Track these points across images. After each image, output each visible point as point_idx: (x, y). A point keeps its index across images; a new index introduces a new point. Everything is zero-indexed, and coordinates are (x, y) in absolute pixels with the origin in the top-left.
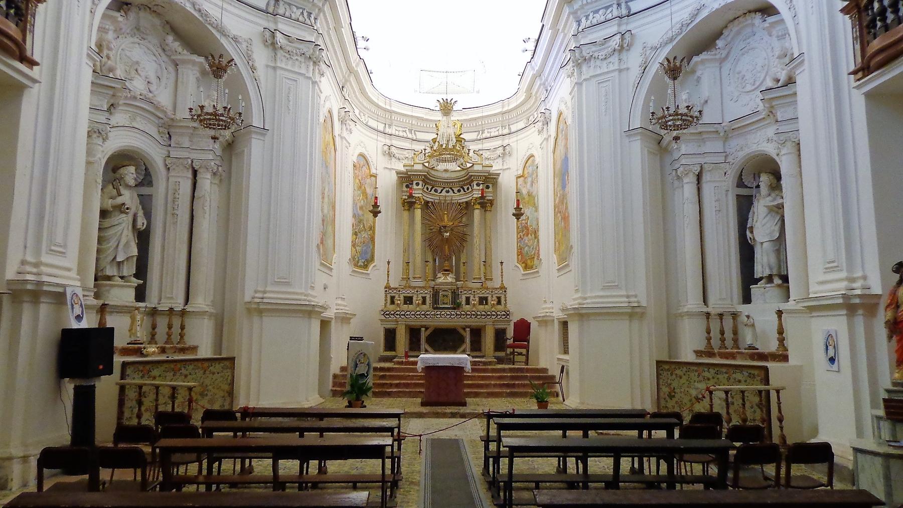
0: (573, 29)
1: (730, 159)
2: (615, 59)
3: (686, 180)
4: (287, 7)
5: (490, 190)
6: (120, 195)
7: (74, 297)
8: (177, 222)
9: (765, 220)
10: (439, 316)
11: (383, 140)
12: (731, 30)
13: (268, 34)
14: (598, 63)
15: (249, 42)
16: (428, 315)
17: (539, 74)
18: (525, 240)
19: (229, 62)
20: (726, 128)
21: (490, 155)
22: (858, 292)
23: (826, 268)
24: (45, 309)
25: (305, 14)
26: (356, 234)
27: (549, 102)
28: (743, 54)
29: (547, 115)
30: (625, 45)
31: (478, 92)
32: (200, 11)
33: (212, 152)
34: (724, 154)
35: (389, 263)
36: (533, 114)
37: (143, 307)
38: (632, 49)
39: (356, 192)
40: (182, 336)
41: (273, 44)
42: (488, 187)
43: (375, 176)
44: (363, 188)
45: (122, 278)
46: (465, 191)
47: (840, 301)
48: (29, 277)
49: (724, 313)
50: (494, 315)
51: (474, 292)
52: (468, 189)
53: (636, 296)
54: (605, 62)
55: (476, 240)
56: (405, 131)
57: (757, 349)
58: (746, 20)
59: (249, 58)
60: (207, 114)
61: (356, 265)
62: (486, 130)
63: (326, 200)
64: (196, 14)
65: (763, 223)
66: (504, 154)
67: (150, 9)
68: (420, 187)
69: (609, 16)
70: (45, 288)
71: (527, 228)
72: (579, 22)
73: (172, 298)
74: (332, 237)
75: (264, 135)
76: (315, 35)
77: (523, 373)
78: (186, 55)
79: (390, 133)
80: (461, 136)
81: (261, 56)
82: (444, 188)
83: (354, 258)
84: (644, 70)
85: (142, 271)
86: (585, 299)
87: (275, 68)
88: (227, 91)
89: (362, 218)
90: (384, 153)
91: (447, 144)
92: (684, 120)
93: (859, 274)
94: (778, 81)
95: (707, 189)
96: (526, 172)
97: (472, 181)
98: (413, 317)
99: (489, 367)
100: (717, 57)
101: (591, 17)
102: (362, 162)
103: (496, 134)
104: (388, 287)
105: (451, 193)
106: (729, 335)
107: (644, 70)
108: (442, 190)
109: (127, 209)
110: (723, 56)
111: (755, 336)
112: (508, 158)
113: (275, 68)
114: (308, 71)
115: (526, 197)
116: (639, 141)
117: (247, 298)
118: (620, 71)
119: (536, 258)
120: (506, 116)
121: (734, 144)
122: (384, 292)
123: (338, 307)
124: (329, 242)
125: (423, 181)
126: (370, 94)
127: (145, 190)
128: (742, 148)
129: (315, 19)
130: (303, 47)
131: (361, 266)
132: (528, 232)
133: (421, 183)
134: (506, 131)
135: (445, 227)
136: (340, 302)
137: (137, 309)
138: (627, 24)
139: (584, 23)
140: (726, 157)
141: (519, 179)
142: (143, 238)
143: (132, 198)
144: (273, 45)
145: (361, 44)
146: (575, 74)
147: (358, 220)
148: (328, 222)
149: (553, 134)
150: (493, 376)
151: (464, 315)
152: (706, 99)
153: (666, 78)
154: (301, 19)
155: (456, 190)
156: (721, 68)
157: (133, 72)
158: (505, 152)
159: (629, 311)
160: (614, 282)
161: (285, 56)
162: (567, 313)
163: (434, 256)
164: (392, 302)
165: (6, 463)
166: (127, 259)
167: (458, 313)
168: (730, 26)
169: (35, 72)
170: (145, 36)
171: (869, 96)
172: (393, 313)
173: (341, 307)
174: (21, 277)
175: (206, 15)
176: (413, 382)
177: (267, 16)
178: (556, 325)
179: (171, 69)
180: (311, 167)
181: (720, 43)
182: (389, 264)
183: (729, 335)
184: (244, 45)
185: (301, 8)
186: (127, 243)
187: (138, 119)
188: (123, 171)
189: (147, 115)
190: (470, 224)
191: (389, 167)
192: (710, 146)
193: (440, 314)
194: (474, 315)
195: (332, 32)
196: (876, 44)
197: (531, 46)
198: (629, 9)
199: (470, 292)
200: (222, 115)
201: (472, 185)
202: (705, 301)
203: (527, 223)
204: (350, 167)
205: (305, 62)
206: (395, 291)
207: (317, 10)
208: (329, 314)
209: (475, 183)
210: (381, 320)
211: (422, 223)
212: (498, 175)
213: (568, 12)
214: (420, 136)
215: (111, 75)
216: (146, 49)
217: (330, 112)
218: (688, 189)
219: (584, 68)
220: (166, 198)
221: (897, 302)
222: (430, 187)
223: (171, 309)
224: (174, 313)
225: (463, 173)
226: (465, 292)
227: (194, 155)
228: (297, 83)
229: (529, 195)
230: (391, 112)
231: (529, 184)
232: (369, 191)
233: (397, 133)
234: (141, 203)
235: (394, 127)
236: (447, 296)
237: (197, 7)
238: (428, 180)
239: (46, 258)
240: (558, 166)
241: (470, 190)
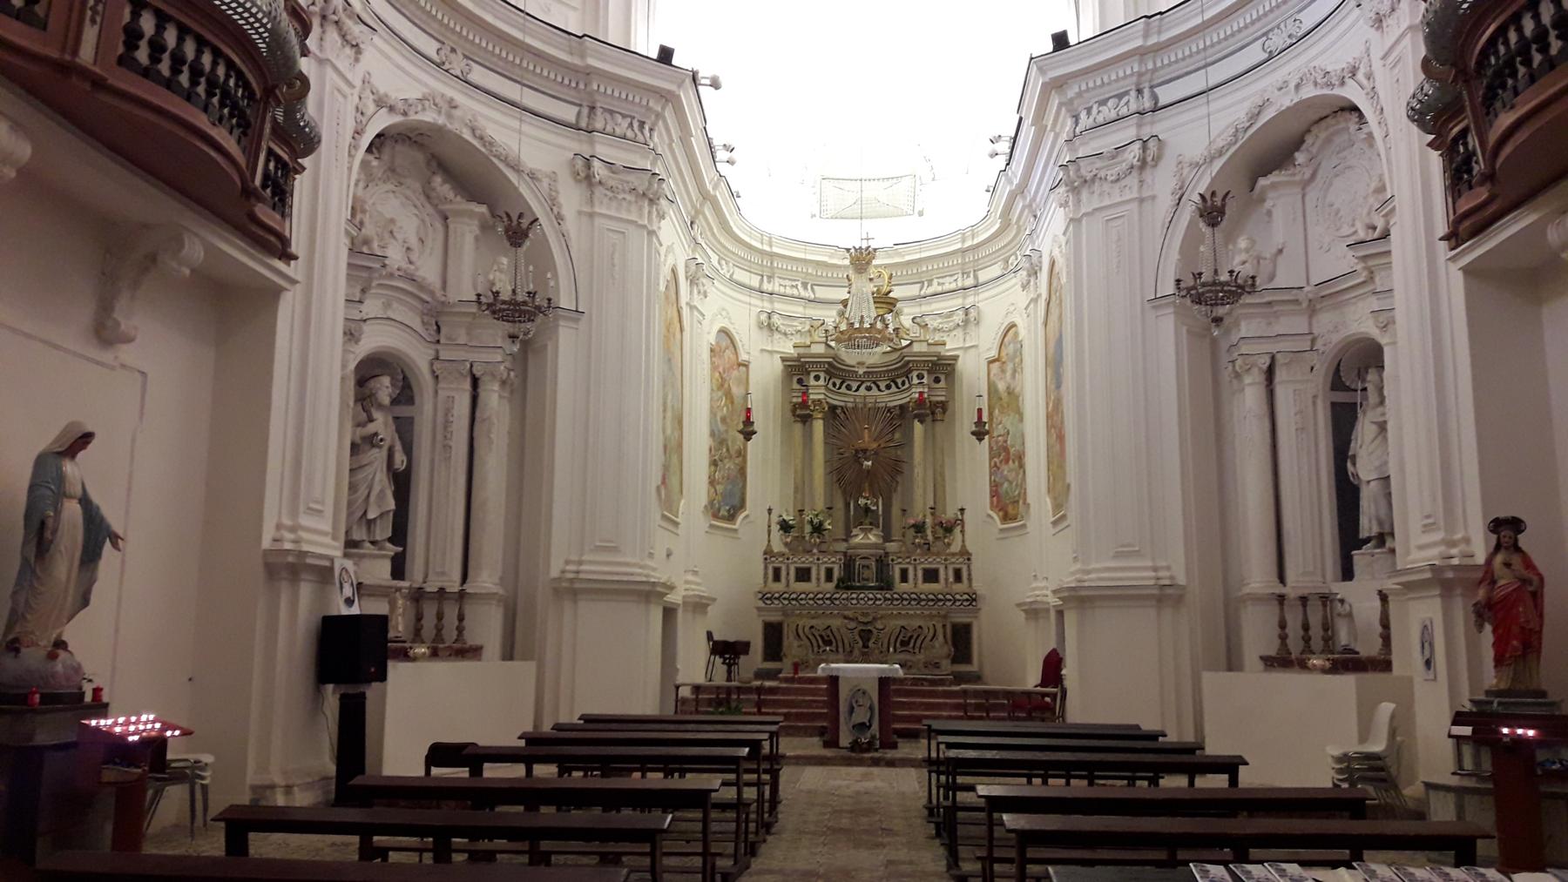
0: (1067, 129)
1: (1318, 345)
2: (1133, 180)
3: (1248, 380)
4: (608, 116)
5: (942, 384)
6: (371, 420)
7: (344, 573)
8: (450, 457)
9: (1373, 446)
10: (854, 602)
11: (758, 303)
12: (1317, 136)
13: (580, 163)
14: (1106, 187)
15: (553, 177)
16: (836, 599)
17: (1021, 190)
18: (1003, 471)
19: (532, 223)
20: (1310, 296)
21: (941, 323)
22: (1455, 561)
23: (1425, 526)
24: (306, 590)
25: (636, 125)
26: (714, 463)
27: (1038, 237)
28: (1337, 175)
29: (1035, 259)
30: (1149, 159)
31: (921, 214)
32: (481, 138)
33: (499, 350)
34: (1310, 337)
35: (770, 511)
36: (1015, 254)
37: (406, 588)
38: (1162, 164)
39: (714, 395)
40: (460, 630)
41: (589, 178)
42: (937, 380)
43: (746, 365)
44: (726, 386)
45: (373, 543)
46: (898, 388)
47: (1428, 575)
48: (288, 546)
49: (1310, 597)
50: (950, 600)
51: (915, 560)
52: (903, 383)
53: (1168, 568)
54: (1118, 184)
55: (918, 471)
56: (796, 287)
57: (1357, 653)
58: (1338, 123)
59: (552, 202)
60: (504, 302)
61: (716, 516)
62: (935, 280)
63: (669, 414)
64: (475, 142)
65: (1370, 450)
66: (966, 322)
67: (410, 138)
68: (821, 382)
69: (1124, 111)
70: (309, 561)
71: (1006, 450)
72: (1076, 118)
73: (443, 573)
74: (678, 473)
75: (577, 320)
76: (651, 157)
77: (998, 699)
78: (461, 204)
79: (770, 289)
80: (891, 295)
81: (571, 199)
82: (863, 382)
83: (711, 503)
84: (1180, 199)
85: (400, 534)
86: (1088, 572)
87: (591, 215)
88: (531, 268)
89: (724, 436)
90: (760, 325)
91: (862, 322)
92: (1226, 292)
93: (1459, 536)
94: (1374, 228)
95: (1281, 393)
96: (1003, 354)
97: (910, 371)
98: (811, 602)
99: (940, 688)
100: (1297, 178)
101: (1094, 111)
102: (725, 342)
103: (953, 286)
104: (768, 553)
105: (875, 391)
106: (1316, 632)
107: (1180, 199)
108: (859, 387)
109: (381, 440)
110: (1307, 176)
111: (1353, 633)
112: (973, 328)
113: (591, 215)
114: (641, 216)
115: (1005, 396)
116: (1172, 316)
117: (554, 573)
118: (1141, 200)
119: (1021, 502)
120: (969, 257)
121: (1325, 322)
122: (762, 560)
123: (688, 586)
124: (674, 481)
125: (827, 372)
126: (735, 229)
127: (403, 411)
128: (1336, 327)
129: (651, 130)
130: (632, 178)
131: (723, 518)
132: (1007, 456)
133: (822, 375)
134: (970, 282)
135: (865, 451)
136: (690, 577)
137: (399, 589)
138: (1152, 123)
139: (1085, 120)
140: (1313, 341)
141: (991, 365)
142: (402, 483)
143: (386, 424)
144: (586, 177)
145: (722, 155)
146: (1070, 203)
147: (719, 440)
148: (673, 448)
149: (1044, 295)
150: (946, 704)
151: (897, 599)
152: (1280, 247)
153: (1202, 225)
154: (630, 134)
155: (882, 385)
156: (1304, 196)
157: (387, 235)
158: (969, 319)
159: (1155, 592)
160: (1133, 546)
161: (606, 195)
162: (1062, 595)
163: (845, 499)
164: (777, 578)
165: (268, 793)
166: (381, 515)
167: (888, 596)
168: (1315, 130)
169: (291, 269)
170: (402, 180)
171: (1467, 271)
172: (777, 595)
173: (693, 587)
174: (277, 546)
175: (491, 144)
176: (811, 711)
177: (579, 134)
178: (1053, 614)
179: (439, 225)
180: (647, 361)
181: (1300, 157)
182: (770, 514)
183: (1316, 632)
184: (545, 182)
185: (630, 116)
186: (382, 491)
187: (395, 305)
188: (372, 384)
189: (408, 300)
190: (908, 442)
191: (769, 349)
192: (1286, 324)
193: (857, 599)
194: (915, 599)
195: (677, 146)
196: (1465, 205)
197: (1004, 147)
198: (1155, 98)
199: (908, 560)
200: (525, 303)
201: (910, 376)
202: (1282, 578)
203: (1006, 441)
204: (706, 355)
205: (636, 202)
206: (781, 559)
207: (653, 117)
208: (675, 598)
209: (915, 374)
210: (759, 609)
211: (826, 443)
212: (955, 358)
213: (1057, 102)
214: (822, 293)
215: (365, 250)
216: (404, 200)
217: (674, 271)
218: (1251, 396)
219: (1085, 194)
220: (434, 421)
221: (1493, 575)
222: (838, 382)
223: (442, 590)
224: (446, 595)
225: (895, 356)
226: (900, 560)
227: (472, 357)
228: (624, 237)
229: (1009, 393)
230: (772, 255)
231: (1009, 374)
232: (737, 391)
233: (782, 290)
234: (398, 431)
235: (777, 280)
236: (868, 567)
237: (478, 133)
238: (835, 371)
239: (305, 521)
240: (1051, 350)
241: (907, 385)
